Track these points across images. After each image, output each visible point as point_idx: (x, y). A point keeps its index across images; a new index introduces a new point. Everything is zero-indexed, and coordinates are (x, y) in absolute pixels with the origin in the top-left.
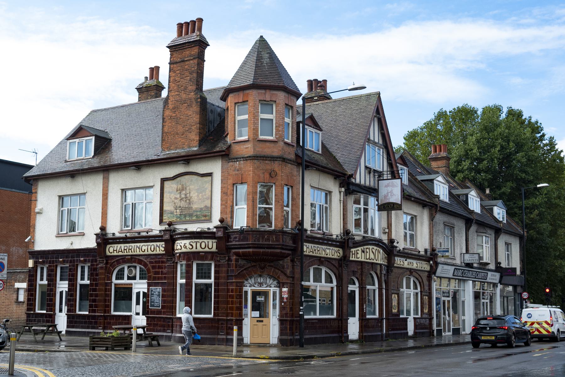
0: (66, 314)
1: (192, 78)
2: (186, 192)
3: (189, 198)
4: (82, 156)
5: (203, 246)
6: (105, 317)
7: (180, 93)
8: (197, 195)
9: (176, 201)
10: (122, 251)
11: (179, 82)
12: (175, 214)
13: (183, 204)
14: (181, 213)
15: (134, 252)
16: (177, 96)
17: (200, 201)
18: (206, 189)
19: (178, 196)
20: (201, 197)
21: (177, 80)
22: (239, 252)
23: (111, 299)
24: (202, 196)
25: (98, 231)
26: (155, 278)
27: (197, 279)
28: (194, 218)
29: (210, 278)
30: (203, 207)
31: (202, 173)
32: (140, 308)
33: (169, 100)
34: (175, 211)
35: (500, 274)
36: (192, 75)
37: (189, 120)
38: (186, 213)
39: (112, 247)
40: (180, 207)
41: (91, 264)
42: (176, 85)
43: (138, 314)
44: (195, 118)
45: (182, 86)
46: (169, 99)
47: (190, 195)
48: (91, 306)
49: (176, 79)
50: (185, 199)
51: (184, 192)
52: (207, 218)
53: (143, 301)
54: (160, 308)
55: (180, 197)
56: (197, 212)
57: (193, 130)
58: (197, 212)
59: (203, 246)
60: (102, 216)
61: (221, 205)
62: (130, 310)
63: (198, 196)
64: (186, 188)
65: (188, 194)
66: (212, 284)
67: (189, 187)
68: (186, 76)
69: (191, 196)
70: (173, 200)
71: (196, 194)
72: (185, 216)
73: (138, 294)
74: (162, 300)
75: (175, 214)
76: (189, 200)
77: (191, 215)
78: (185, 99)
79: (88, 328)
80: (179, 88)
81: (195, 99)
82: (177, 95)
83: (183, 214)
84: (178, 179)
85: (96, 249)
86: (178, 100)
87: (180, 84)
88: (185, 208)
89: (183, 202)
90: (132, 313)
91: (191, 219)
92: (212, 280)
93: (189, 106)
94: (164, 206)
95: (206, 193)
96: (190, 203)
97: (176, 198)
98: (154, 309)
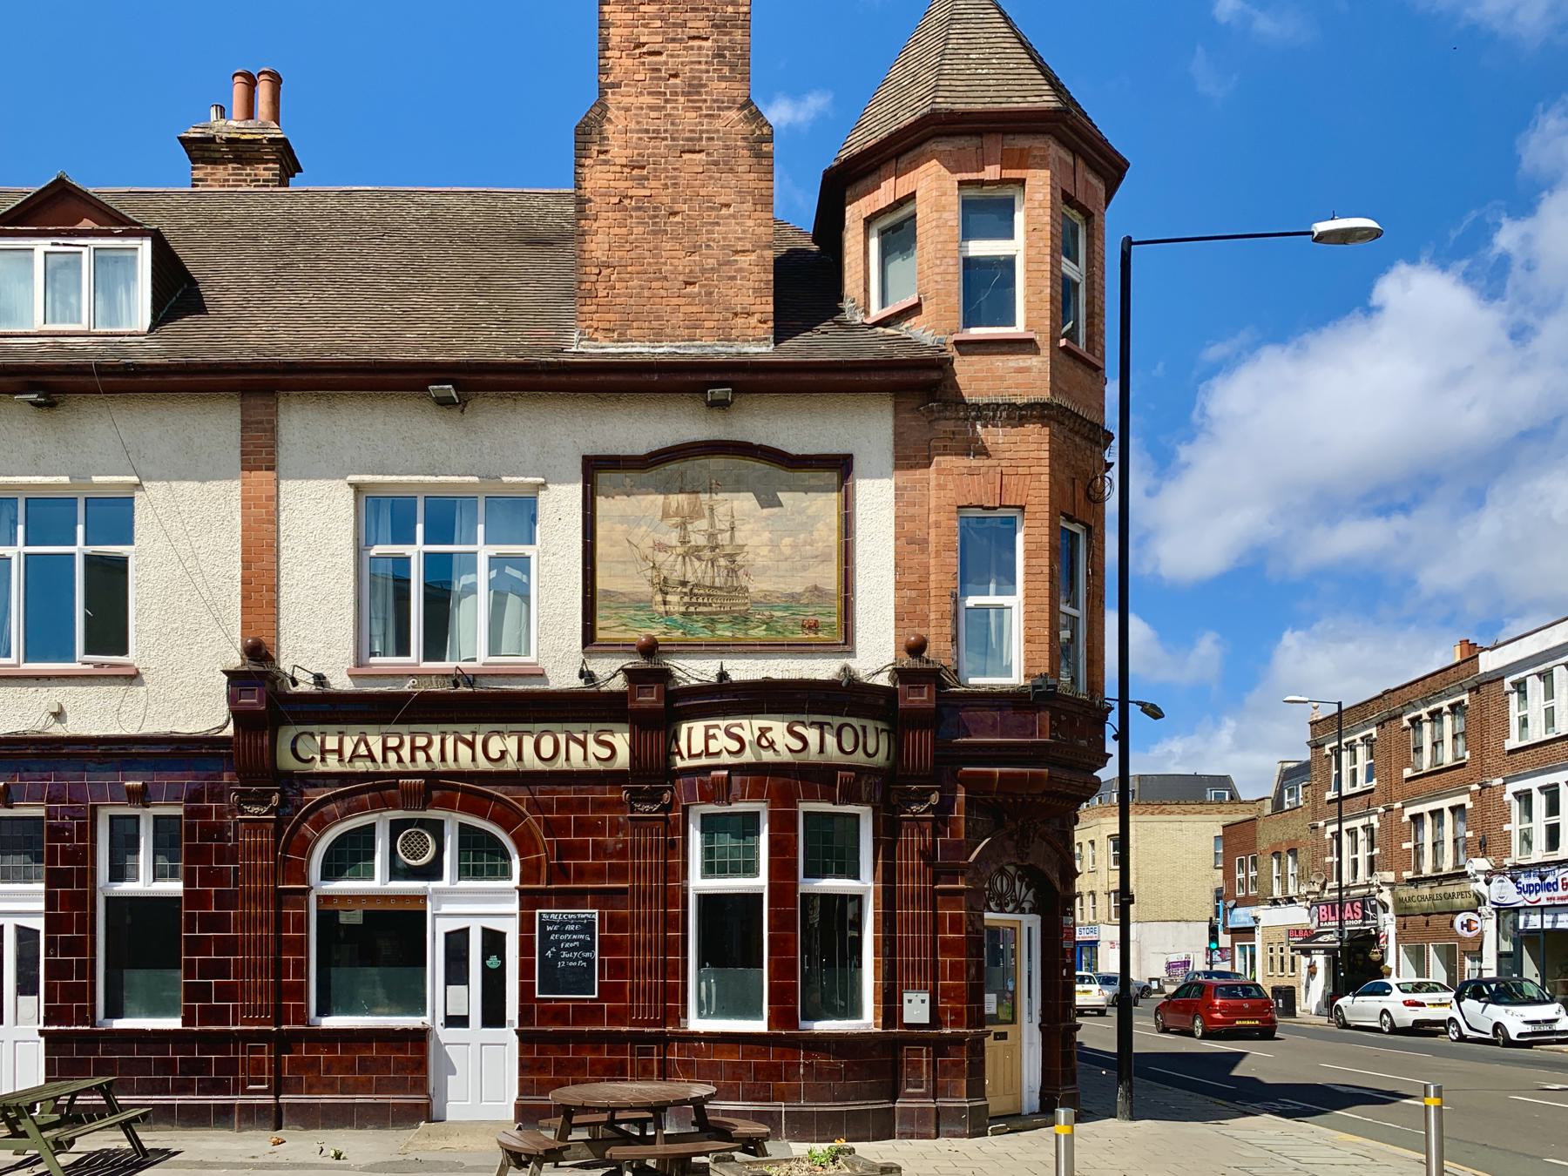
0: (41, 1033)
1: (725, 48)
2: (712, 525)
3: (728, 550)
4: (1012, 323)
5: (546, 750)
6: (284, 1042)
7: (667, 101)
8: (771, 540)
9: (660, 557)
10: (371, 757)
11: (659, 53)
12: (662, 609)
13: (696, 571)
14: (692, 609)
15: (443, 759)
16: (653, 114)
17: (784, 565)
18: (815, 518)
19: (673, 538)
20: (787, 551)
21: (644, 44)
22: (992, 774)
23: (93, 962)
24: (794, 546)
25: (235, 660)
26: (558, 873)
27: (372, 878)
28: (759, 633)
29: (750, 869)
30: (799, 589)
31: (794, 450)
32: (470, 999)
33: (607, 126)
34: (659, 598)
35: (128, 856)
36: (726, 34)
37: (718, 224)
38: (714, 608)
39: (312, 735)
40: (684, 584)
41: (48, 810)
42: (644, 63)
43: (460, 1021)
44: (750, 223)
45: (675, 76)
46: (609, 120)
47: (732, 538)
48: (192, 992)
49: (643, 39)
50: (707, 554)
51: (703, 524)
52: (820, 635)
53: (484, 966)
54: (596, 996)
55: (683, 543)
56: (772, 607)
57: (740, 270)
58: (772, 607)
59: (546, 750)
60: (245, 598)
61: (899, 586)
62: (418, 1006)
63: (774, 545)
64: (712, 509)
65: (722, 531)
66: (762, 895)
67: (728, 506)
68: (693, 33)
69: (739, 540)
70: (648, 552)
71: (766, 535)
72: (712, 622)
73: (457, 942)
74: (601, 962)
75: (662, 609)
76: (731, 558)
77: (743, 619)
78: (691, 131)
79: (364, 1088)
80: (660, 78)
81: (744, 139)
82: (652, 108)
83: (697, 613)
84: (672, 467)
85: (226, 739)
86: (658, 132)
87: (666, 63)
88: (712, 587)
89: (697, 564)
90: (430, 1018)
91: (740, 635)
92: (760, 882)
93: (716, 163)
94: (599, 573)
95: (816, 535)
96: (732, 572)
97: (661, 547)
98: (557, 1000)
